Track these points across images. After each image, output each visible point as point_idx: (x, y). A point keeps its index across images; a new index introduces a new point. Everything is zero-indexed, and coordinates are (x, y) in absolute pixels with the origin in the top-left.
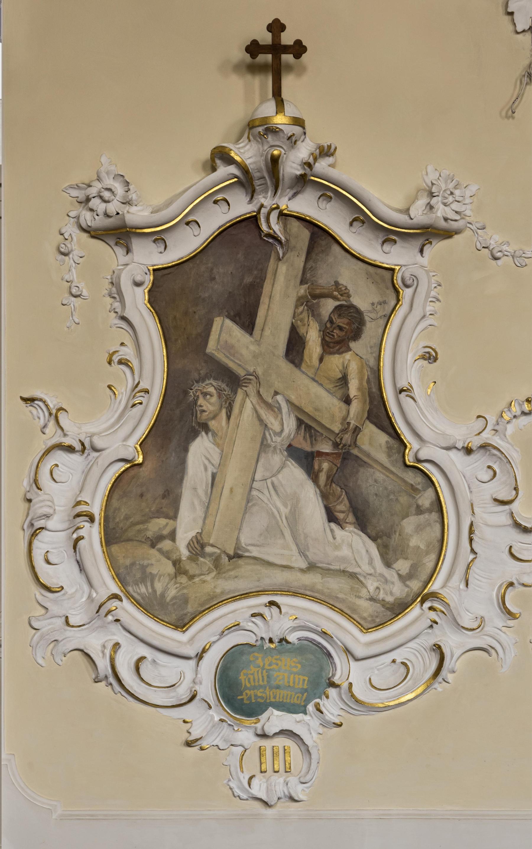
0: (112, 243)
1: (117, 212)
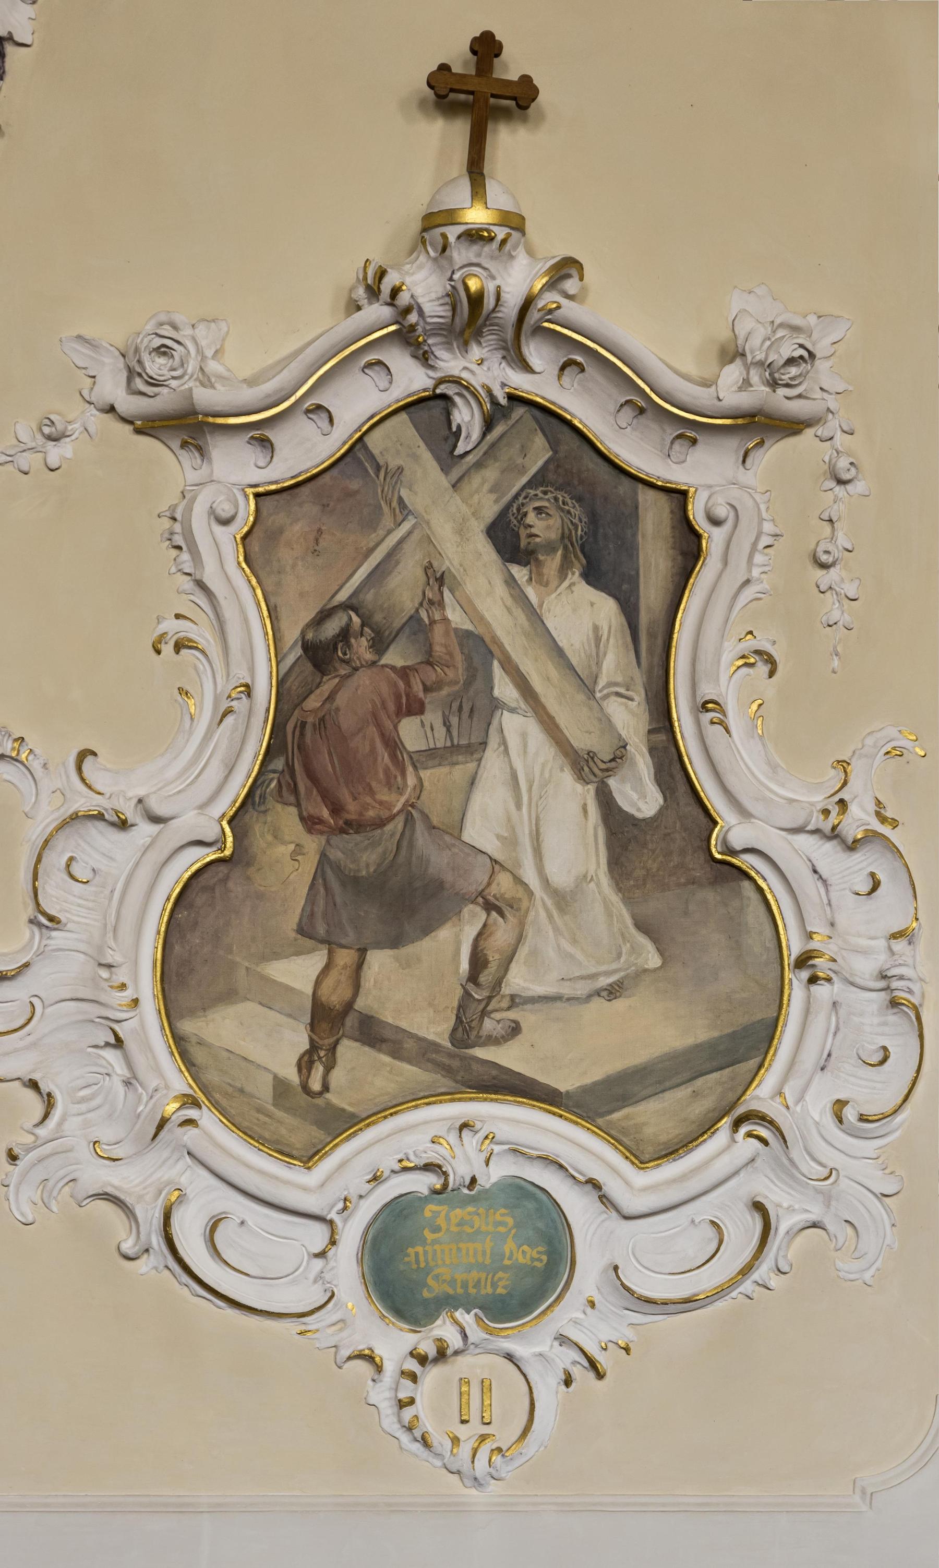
0: (175, 444)
1: (830, 516)
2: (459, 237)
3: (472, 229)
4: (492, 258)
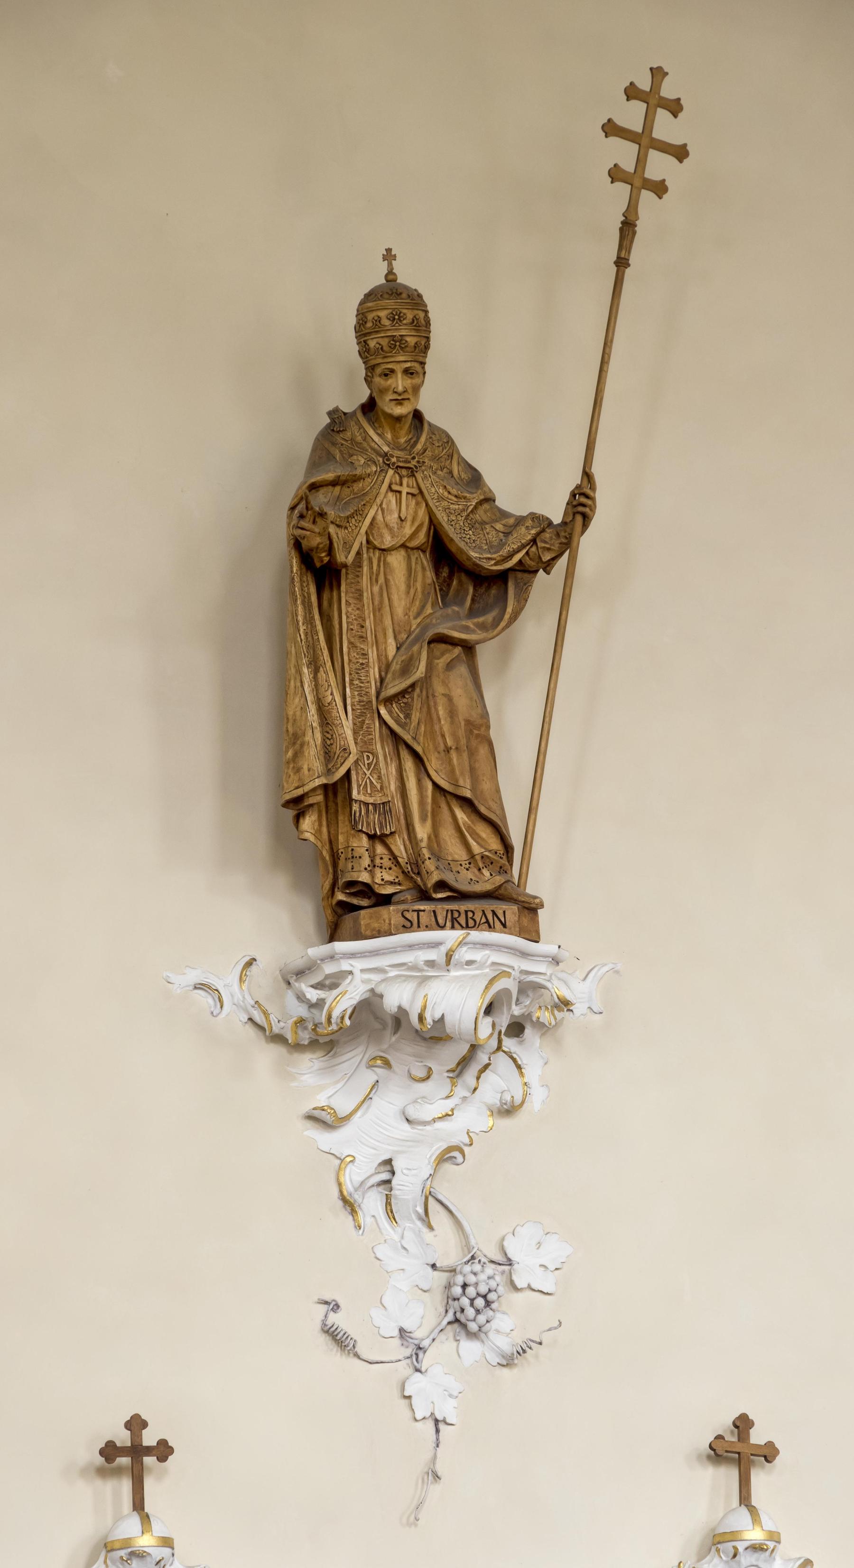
2: (746, 1549)
3: (756, 1544)
4: (765, 1561)
